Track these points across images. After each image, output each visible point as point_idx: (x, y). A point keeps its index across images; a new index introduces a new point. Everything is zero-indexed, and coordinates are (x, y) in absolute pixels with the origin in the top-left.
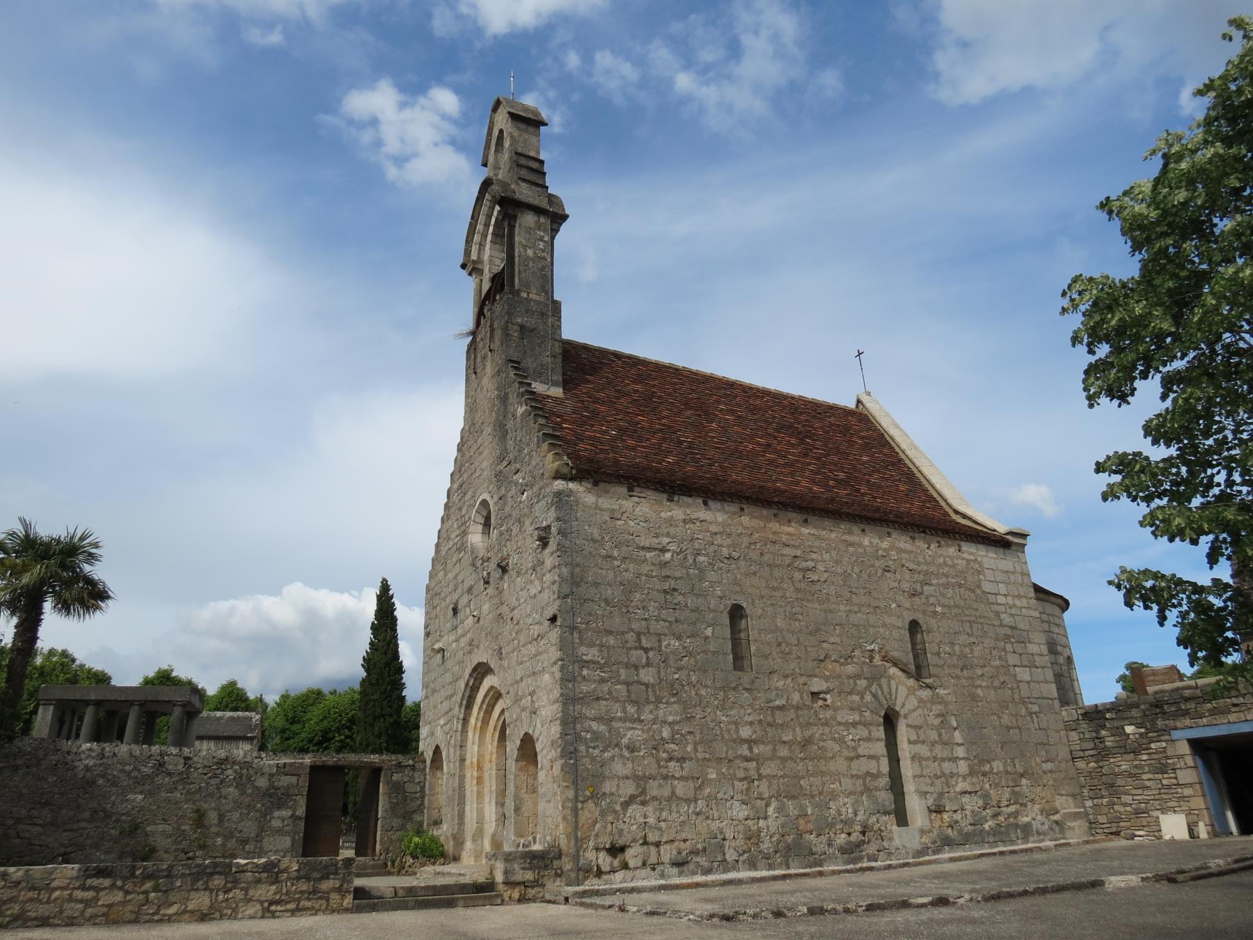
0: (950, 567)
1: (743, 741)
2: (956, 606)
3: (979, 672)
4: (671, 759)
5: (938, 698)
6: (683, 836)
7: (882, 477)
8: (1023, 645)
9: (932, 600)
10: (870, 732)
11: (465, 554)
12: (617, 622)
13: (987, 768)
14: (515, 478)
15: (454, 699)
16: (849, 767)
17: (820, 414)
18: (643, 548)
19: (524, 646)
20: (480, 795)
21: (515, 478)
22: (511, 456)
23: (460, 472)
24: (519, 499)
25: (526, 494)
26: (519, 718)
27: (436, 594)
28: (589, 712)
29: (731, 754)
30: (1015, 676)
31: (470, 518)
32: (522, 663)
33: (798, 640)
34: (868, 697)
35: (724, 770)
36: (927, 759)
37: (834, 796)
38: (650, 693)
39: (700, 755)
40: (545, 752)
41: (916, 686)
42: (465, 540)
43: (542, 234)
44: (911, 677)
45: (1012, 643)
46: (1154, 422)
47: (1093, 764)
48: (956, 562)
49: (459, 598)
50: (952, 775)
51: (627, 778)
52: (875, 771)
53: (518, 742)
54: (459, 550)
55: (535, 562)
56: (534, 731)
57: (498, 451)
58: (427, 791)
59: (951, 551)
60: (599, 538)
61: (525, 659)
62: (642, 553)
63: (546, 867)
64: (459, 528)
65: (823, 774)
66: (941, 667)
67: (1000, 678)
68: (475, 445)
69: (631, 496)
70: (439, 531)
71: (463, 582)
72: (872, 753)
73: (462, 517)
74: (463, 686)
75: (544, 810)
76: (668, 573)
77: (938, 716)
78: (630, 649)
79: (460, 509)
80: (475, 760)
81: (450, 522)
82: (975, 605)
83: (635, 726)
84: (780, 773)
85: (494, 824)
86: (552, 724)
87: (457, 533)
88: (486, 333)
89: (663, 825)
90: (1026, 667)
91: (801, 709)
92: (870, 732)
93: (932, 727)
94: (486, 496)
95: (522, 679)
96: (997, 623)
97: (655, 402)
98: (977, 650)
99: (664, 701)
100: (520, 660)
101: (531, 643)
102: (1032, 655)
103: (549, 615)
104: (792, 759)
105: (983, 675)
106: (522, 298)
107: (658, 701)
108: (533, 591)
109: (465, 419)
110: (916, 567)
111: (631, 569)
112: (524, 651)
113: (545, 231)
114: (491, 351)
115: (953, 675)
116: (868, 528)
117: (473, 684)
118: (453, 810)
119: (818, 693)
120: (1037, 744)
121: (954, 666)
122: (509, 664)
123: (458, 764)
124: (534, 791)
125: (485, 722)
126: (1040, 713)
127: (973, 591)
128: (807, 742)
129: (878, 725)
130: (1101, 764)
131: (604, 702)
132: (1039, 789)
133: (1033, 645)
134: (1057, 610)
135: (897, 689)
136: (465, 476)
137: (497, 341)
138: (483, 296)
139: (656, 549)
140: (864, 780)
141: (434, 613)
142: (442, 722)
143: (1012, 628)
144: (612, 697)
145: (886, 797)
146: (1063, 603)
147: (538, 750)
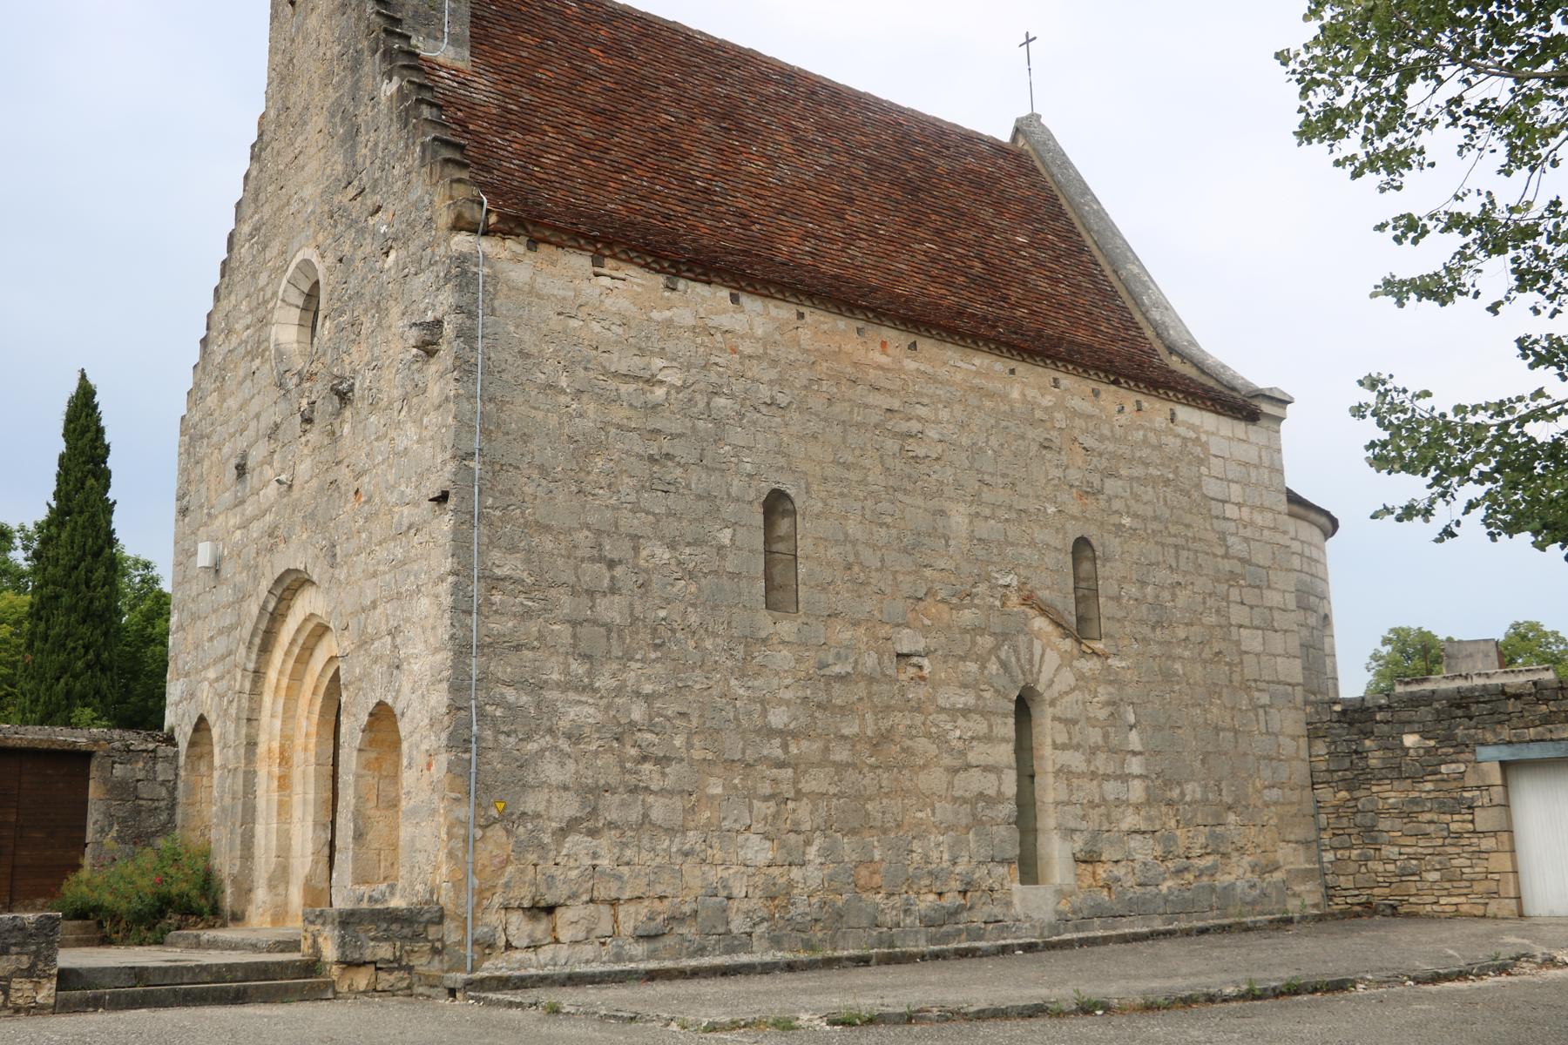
0: (1154, 448)
2: (1155, 518)
3: (1181, 633)
4: (645, 759)
6: (659, 889)
10: (990, 727)
16: (951, 784)
18: (615, 375)
20: (283, 808)
21: (371, 222)
23: (256, 200)
24: (378, 265)
25: (393, 255)
29: (750, 756)
30: (1238, 643)
31: (275, 294)
32: (375, 575)
33: (882, 560)
34: (993, 667)
35: (736, 781)
39: (697, 754)
41: (1075, 652)
44: (1067, 636)
47: (1343, 794)
49: (250, 446)
50: (1119, 803)
53: (364, 719)
54: (252, 355)
55: (409, 388)
56: (396, 698)
63: (416, 937)
64: (251, 311)
66: (1118, 620)
68: (290, 150)
69: (597, 275)
71: (257, 416)
72: (990, 761)
74: (255, 610)
76: (658, 426)
79: (254, 275)
80: (276, 745)
81: (233, 298)
82: (1188, 519)
83: (583, 699)
84: (833, 790)
85: (310, 858)
87: (249, 319)
89: (625, 870)
91: (877, 681)
92: (990, 727)
94: (310, 253)
95: (374, 605)
96: (1220, 551)
98: (1183, 596)
102: (1271, 609)
104: (854, 766)
105: (1187, 638)
111: (591, 414)
112: (381, 554)
115: (1138, 636)
116: (1021, 368)
117: (275, 608)
119: (908, 656)
123: (242, 751)
125: (297, 677)
129: (1005, 715)
130: (1357, 794)
132: (1253, 831)
133: (1274, 593)
134: (1316, 534)
135: (1042, 656)
136: (267, 211)
139: (637, 378)
140: (974, 807)
141: (198, 471)
142: (212, 674)
143: (1243, 561)
145: (1007, 838)
147: (402, 734)
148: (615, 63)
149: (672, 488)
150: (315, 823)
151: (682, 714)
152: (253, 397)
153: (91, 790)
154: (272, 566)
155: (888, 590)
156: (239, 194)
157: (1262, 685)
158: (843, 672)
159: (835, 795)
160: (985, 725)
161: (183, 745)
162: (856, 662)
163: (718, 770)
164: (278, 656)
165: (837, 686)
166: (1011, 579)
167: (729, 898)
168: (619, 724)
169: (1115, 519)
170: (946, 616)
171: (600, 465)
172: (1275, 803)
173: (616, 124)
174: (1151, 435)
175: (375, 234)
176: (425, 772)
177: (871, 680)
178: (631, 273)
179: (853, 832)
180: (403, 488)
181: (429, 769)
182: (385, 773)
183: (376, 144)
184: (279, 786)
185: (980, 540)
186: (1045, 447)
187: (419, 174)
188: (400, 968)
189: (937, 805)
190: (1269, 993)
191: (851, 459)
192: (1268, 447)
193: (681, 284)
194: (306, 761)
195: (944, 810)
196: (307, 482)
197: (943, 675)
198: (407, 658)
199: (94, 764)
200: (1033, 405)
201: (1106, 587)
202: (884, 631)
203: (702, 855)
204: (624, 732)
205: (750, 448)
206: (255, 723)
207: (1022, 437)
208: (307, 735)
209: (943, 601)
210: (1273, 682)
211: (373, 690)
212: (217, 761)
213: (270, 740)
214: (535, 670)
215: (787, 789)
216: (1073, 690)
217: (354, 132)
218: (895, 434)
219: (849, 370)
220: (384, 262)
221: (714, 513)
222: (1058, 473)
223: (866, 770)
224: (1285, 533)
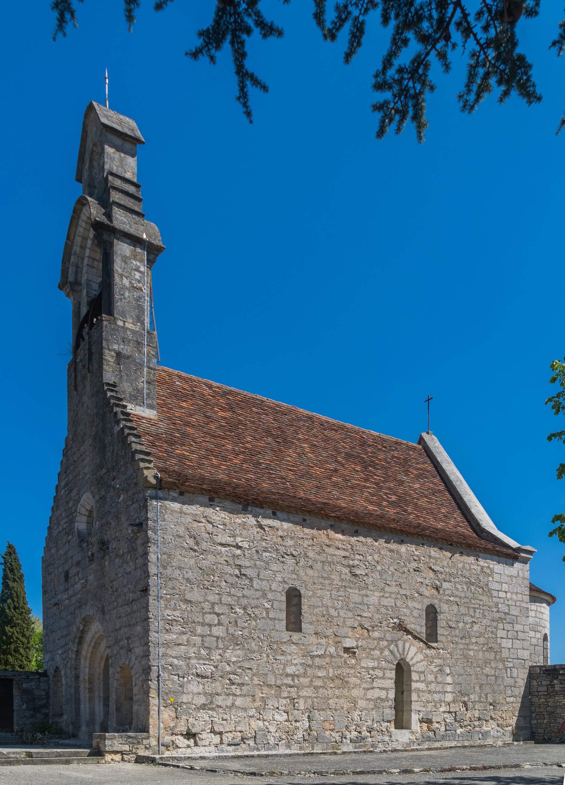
0: (467, 570)
6: (239, 728)
7: (427, 501)
8: (511, 625)
11: (73, 537)
16: (365, 694)
17: (385, 447)
19: (121, 606)
20: (91, 699)
23: (66, 472)
29: (279, 682)
30: (500, 644)
32: (120, 617)
33: (338, 613)
34: (386, 653)
36: (423, 691)
43: (138, 264)
48: (472, 567)
49: (69, 569)
50: (441, 701)
51: (199, 694)
52: (384, 697)
54: (68, 534)
56: (129, 662)
57: (98, 460)
59: (471, 559)
62: (219, 548)
64: (67, 517)
70: (51, 518)
71: (72, 557)
76: (239, 563)
78: (206, 613)
79: (67, 502)
80: (87, 677)
81: (59, 511)
82: (481, 597)
84: (314, 695)
87: (66, 520)
88: (85, 355)
89: (224, 722)
90: (510, 639)
91: (335, 657)
95: (120, 628)
96: (495, 610)
97: (241, 428)
98: (476, 627)
100: (118, 616)
101: (127, 604)
102: (517, 632)
105: (477, 642)
106: (119, 326)
113: (141, 261)
115: (454, 642)
116: (406, 539)
117: (83, 629)
119: (349, 648)
121: (456, 636)
123: (73, 679)
124: (131, 699)
129: (391, 670)
131: (184, 647)
135: (409, 649)
136: (71, 477)
138: (81, 319)
139: (229, 545)
142: (60, 652)
143: (506, 614)
145: (390, 713)
146: (550, 600)
148: (228, 414)
152: (69, 550)
153: (14, 692)
155: (341, 624)
156: (59, 470)
157: (509, 660)
161: (51, 677)
162: (326, 650)
167: (268, 732)
173: (226, 441)
175: (114, 488)
177: (331, 656)
180: (129, 586)
183: (113, 451)
188: (132, 753)
191: (326, 575)
198: (133, 648)
199: (14, 683)
204: (224, 674)
209: (365, 629)
212: (64, 682)
215: (294, 695)
223: (329, 689)
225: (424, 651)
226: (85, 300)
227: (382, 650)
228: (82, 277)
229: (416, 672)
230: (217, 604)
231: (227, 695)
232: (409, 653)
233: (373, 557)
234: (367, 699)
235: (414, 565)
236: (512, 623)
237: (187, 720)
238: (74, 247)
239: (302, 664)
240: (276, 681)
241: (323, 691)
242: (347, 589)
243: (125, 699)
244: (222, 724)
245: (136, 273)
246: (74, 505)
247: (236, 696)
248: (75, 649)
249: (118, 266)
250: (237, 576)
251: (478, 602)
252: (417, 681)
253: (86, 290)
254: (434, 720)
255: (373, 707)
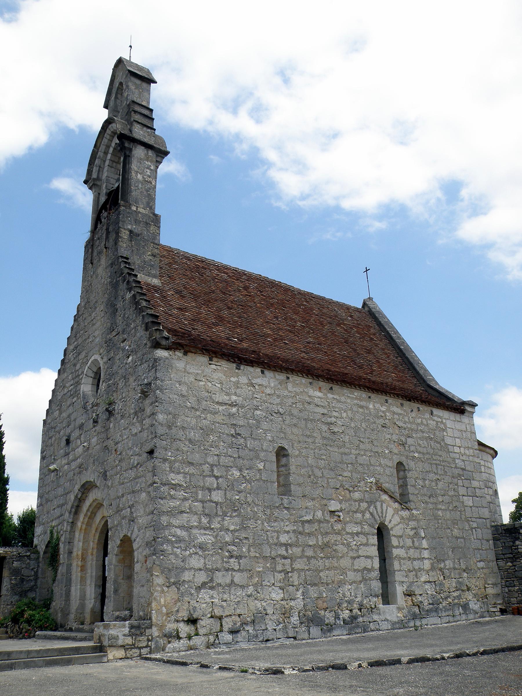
0: (425, 425)
1: (282, 545)
2: (427, 453)
3: (440, 499)
4: (231, 557)
5: (413, 517)
6: (238, 612)
8: (469, 481)
9: (412, 448)
10: (367, 539)
11: (78, 399)
12: (197, 457)
13: (442, 565)
14: (122, 345)
15: (64, 507)
16: (353, 564)
18: (218, 403)
20: (83, 579)
21: (122, 345)
22: (120, 329)
23: (75, 337)
24: (125, 361)
25: (130, 358)
26: (120, 524)
27: (52, 428)
28: (175, 522)
29: (274, 554)
30: (463, 502)
31: (83, 372)
32: (123, 484)
33: (322, 473)
34: (368, 516)
35: (268, 565)
37: (341, 583)
38: (219, 509)
39: (252, 554)
40: (140, 550)
41: (399, 508)
42: (78, 389)
44: (396, 502)
45: (462, 479)
46: (279, 204)
47: (510, 564)
49: (72, 432)
50: (420, 569)
51: (200, 570)
53: (119, 542)
55: (137, 409)
56: (132, 534)
58: (40, 575)
60: (186, 394)
61: (126, 481)
62: (217, 407)
63: (141, 634)
64: (73, 379)
65: (336, 568)
66: (416, 495)
67: (454, 503)
68: (89, 318)
69: (210, 364)
71: (75, 420)
72: (368, 554)
73: (76, 371)
74: (73, 498)
75: (139, 593)
76: (234, 422)
77: (412, 529)
78: (206, 476)
79: (75, 365)
80: (80, 553)
82: (440, 453)
83: (207, 533)
85: (93, 601)
86: (147, 529)
87: (72, 382)
89: (224, 604)
90: (470, 496)
91: (322, 522)
92: (367, 539)
93: (409, 537)
94: (97, 357)
95: (123, 496)
98: (440, 485)
99: (228, 515)
101: (131, 469)
102: (475, 488)
103: (148, 449)
104: (314, 557)
105: (443, 501)
107: (225, 514)
108: (134, 431)
109: (82, 298)
110: (403, 425)
111: (208, 418)
112: (126, 475)
113: (151, 162)
114: (106, 248)
115: (424, 501)
116: (373, 396)
117: (81, 497)
118: (61, 590)
119: (334, 512)
120: (475, 549)
121: (425, 495)
122: (112, 484)
123: (66, 556)
125: (89, 525)
126: (477, 528)
127: (439, 443)
128: (327, 545)
129: (373, 535)
130: (515, 563)
132: (474, 580)
133: (476, 481)
134: (490, 458)
135: (386, 510)
136: (80, 341)
137: (111, 241)
138: (100, 207)
139: (226, 404)
140: (363, 573)
141: (50, 441)
143: (463, 469)
144: (191, 511)
145: (376, 585)
147: (135, 548)
149: (240, 447)
150: (96, 586)
151: (246, 538)
152: (73, 413)
154: (80, 480)
155: (325, 485)
157: (473, 519)
158: (309, 519)
159: (307, 570)
160: (365, 539)
162: (314, 515)
163: (260, 561)
164: (81, 517)
165: (306, 525)
166: (372, 480)
167: (266, 614)
168: (221, 543)
169: (411, 454)
170: (348, 495)
171: (212, 438)
172: (482, 568)
174: (424, 420)
176: (144, 564)
177: (320, 522)
178: (223, 363)
179: (315, 585)
181: (146, 563)
182: (126, 565)
183: (124, 315)
184: (81, 570)
185: (360, 464)
186: (383, 427)
187: (141, 327)
189: (348, 573)
190: (492, 651)
192: (469, 424)
193: (242, 367)
194: (92, 559)
195: (351, 575)
196: (95, 446)
197: (348, 519)
198: (137, 516)
200: (378, 410)
201: (411, 481)
202: (324, 502)
203: (255, 596)
205: (270, 430)
206: (72, 544)
207: (375, 423)
208: (93, 549)
209: (347, 489)
210: (477, 518)
211: (122, 530)
213: (78, 551)
214: (187, 521)
216: (399, 524)
217: (115, 311)
218: (326, 423)
219: (307, 398)
220: (128, 360)
221: (257, 457)
222: (389, 436)
223: (319, 559)
224: (478, 457)
225: (399, 512)
226: (105, 192)
227: (363, 513)
228: (102, 175)
229: (395, 536)
230: (216, 465)
231: (226, 570)
232: (387, 515)
233: (347, 414)
234: (355, 570)
235: (381, 421)
236: (469, 479)
237: (189, 602)
238: (99, 153)
239: (294, 531)
240: (271, 552)
241: (314, 562)
242: (328, 447)
243: (123, 579)
244: (222, 606)
245: (147, 170)
246: (81, 367)
247: (235, 570)
248: (71, 520)
249: (134, 166)
250: (232, 435)
251: (439, 458)
252: (397, 547)
253: (105, 184)
254: (416, 593)
255: (361, 579)
